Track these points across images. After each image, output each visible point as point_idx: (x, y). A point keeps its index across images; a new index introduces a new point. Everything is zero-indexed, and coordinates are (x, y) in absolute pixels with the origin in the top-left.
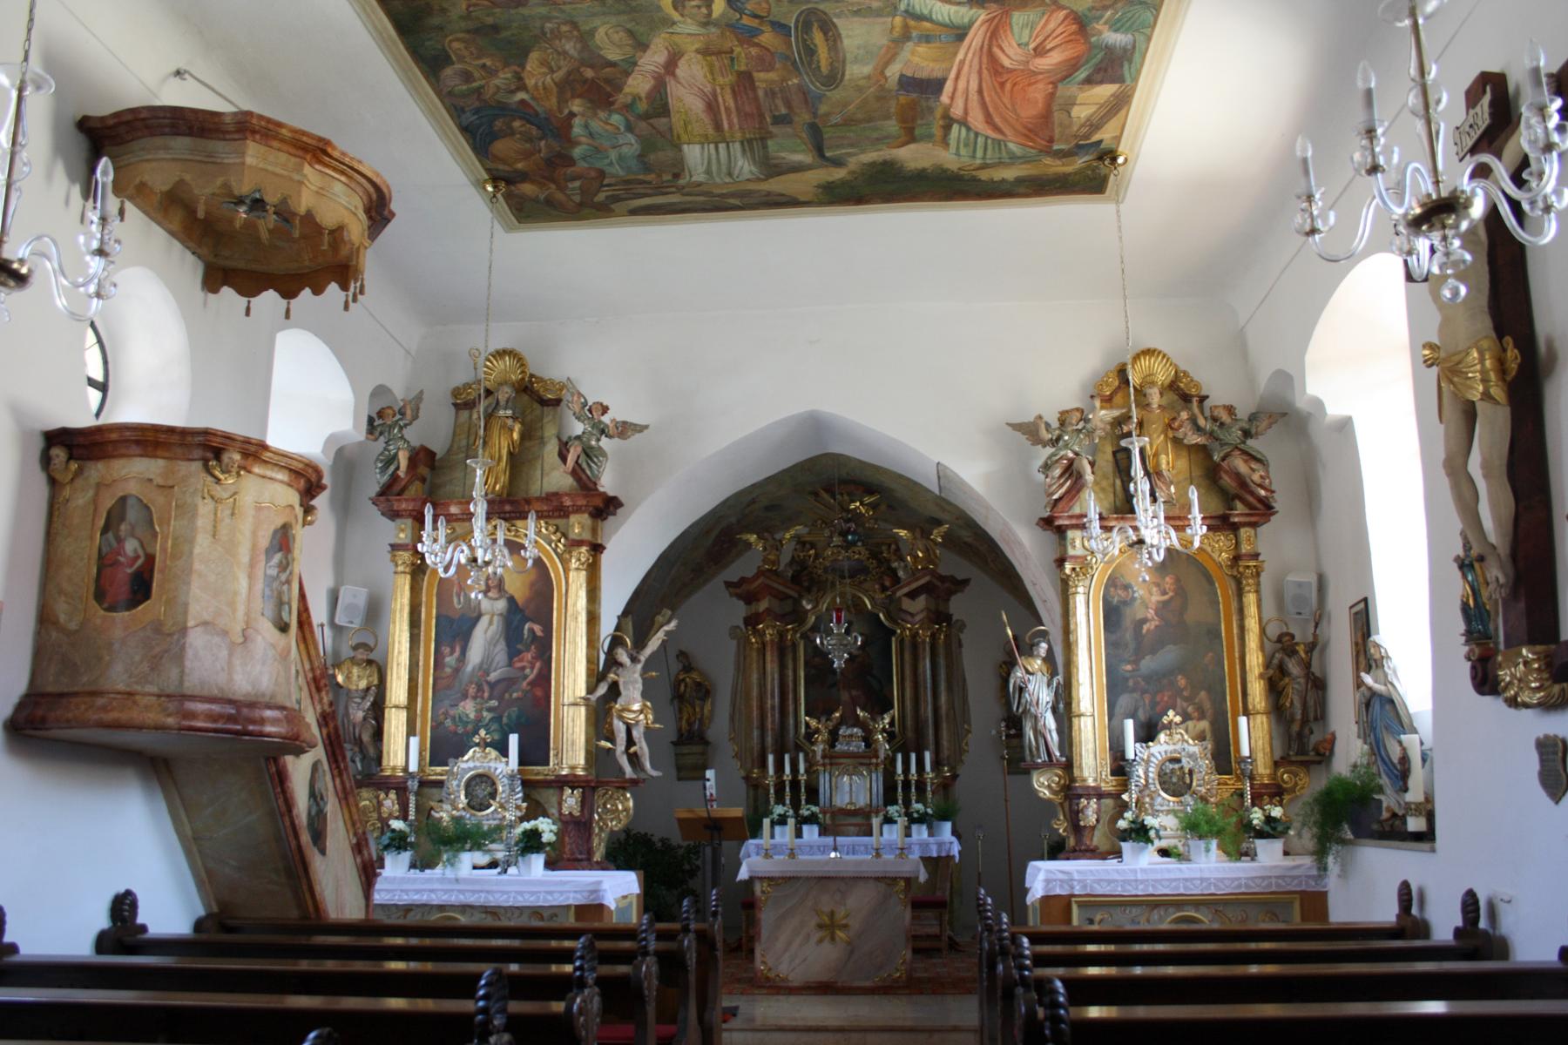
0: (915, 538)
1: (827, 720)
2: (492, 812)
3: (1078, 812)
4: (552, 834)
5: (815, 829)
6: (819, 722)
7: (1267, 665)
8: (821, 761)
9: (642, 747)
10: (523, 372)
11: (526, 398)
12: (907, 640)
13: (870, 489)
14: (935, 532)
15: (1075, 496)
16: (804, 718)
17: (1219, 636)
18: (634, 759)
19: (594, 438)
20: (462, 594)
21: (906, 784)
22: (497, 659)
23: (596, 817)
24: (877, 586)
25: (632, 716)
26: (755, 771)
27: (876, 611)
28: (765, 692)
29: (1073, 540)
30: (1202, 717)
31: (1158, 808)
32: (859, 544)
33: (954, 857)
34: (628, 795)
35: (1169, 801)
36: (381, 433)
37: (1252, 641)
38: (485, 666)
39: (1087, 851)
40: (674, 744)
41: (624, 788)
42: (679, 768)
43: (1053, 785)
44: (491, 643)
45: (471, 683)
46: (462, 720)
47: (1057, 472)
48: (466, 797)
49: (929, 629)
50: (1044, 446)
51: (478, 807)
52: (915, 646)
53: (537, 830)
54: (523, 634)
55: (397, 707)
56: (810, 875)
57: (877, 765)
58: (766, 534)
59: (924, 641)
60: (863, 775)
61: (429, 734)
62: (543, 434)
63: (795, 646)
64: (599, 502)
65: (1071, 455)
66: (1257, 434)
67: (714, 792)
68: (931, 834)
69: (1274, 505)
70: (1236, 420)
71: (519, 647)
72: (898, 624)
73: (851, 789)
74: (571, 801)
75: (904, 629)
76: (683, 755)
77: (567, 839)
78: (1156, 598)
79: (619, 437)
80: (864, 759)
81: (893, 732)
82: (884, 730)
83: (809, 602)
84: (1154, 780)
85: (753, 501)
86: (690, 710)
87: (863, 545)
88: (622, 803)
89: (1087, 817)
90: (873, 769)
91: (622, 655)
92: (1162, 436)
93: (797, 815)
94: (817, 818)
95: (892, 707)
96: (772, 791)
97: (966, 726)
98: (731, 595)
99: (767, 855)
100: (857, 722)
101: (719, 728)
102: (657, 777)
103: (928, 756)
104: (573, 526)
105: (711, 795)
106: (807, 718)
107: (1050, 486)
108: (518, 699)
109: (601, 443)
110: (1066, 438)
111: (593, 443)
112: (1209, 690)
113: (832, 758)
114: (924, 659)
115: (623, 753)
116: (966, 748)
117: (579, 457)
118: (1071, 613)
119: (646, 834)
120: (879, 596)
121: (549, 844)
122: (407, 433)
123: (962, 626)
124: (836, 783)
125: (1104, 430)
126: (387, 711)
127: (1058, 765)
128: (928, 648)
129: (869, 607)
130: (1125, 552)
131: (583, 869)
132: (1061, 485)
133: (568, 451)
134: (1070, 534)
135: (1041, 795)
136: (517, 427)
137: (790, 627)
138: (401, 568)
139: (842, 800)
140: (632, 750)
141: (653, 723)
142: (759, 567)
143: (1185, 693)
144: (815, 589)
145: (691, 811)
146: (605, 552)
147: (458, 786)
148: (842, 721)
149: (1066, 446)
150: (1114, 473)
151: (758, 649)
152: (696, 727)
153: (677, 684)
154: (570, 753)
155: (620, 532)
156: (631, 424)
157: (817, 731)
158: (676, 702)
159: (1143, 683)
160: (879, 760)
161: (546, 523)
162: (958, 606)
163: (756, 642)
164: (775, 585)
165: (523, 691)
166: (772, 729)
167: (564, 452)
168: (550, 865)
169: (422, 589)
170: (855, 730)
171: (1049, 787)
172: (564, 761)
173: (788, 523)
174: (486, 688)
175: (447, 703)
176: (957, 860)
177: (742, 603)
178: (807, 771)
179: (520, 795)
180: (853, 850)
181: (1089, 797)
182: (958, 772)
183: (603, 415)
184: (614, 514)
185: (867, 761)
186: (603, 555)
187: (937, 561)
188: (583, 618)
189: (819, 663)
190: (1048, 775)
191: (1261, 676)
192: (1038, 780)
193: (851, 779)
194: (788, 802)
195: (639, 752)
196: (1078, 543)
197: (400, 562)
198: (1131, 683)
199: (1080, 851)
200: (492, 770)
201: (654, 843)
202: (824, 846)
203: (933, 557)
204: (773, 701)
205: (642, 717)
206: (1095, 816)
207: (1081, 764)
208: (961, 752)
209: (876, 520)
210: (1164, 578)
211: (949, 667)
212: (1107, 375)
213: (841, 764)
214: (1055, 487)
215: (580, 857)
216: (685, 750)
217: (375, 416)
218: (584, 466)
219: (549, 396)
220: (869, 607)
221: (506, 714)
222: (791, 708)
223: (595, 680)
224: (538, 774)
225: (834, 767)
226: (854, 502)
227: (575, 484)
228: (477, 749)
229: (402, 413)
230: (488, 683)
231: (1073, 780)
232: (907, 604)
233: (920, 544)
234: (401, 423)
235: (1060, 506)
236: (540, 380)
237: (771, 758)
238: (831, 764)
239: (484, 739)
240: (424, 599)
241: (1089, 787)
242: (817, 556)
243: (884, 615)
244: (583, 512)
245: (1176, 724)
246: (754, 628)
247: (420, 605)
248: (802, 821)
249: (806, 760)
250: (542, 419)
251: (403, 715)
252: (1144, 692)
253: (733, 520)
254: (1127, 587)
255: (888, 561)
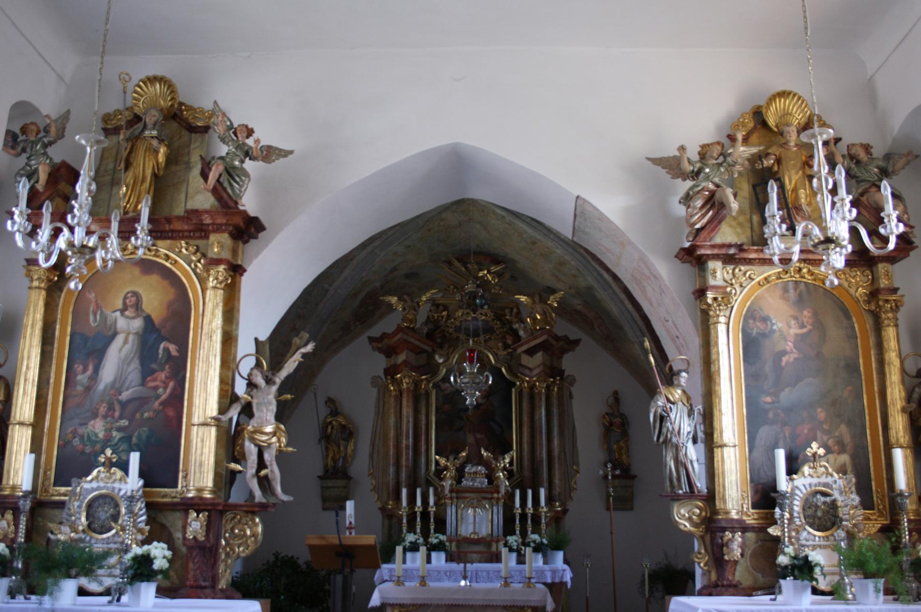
0: (534, 302)
1: (455, 459)
2: (113, 536)
3: (722, 546)
4: (165, 561)
5: (443, 555)
6: (448, 460)
7: (909, 399)
8: (449, 495)
9: (274, 471)
10: (173, 99)
11: (175, 125)
12: (526, 391)
13: (496, 259)
14: (552, 298)
15: (716, 227)
16: (434, 457)
17: (858, 370)
18: (265, 483)
19: (238, 158)
20: (99, 312)
21: (523, 516)
22: (130, 378)
23: (223, 542)
24: (500, 344)
25: (264, 438)
26: (391, 502)
27: (498, 365)
28: (401, 434)
29: (715, 272)
30: (842, 450)
31: (804, 542)
32: (486, 307)
33: (566, 583)
34: (257, 520)
35: (815, 536)
36: (24, 150)
37: (894, 377)
38: (117, 385)
39: (729, 586)
40: (320, 477)
41: (253, 513)
42: (324, 499)
43: (694, 517)
44: (124, 363)
45: (102, 401)
46: (90, 439)
47: (699, 203)
48: (87, 519)
49: (545, 381)
50: (684, 180)
51: (99, 529)
52: (532, 397)
53: (149, 555)
54: (157, 354)
55: (21, 424)
56: (440, 603)
57: (498, 499)
58: (405, 296)
59: (540, 392)
60: (485, 507)
61: (55, 453)
62: (189, 159)
63: (428, 394)
64: (238, 221)
65: (711, 186)
66: (894, 172)
67: (353, 520)
68: (545, 563)
69: (914, 240)
70: (873, 159)
71: (154, 366)
72: (517, 377)
73: (475, 520)
74: (196, 525)
75: (523, 381)
76: (328, 488)
77: (191, 565)
78: (794, 331)
79: (263, 161)
80: (487, 494)
81: (512, 470)
82: (505, 468)
83: (440, 357)
84: (798, 513)
85: (395, 269)
86: (336, 449)
87: (489, 308)
88: (251, 528)
89: (733, 550)
90: (495, 503)
91: (256, 376)
92: (801, 172)
93: (426, 543)
94: (444, 545)
95: (511, 449)
96: (405, 521)
97: (575, 467)
98: (374, 349)
99: (399, 582)
100: (481, 461)
101: (360, 466)
102: (287, 502)
103: (542, 492)
104: (213, 244)
105: (350, 523)
106: (437, 457)
107: (692, 216)
108: (149, 418)
109: (245, 166)
110: (707, 170)
111: (237, 163)
112: (849, 423)
113: (459, 493)
114: (540, 407)
115: (253, 476)
116: (575, 486)
117: (220, 175)
118: (712, 343)
119: (292, 557)
120: (502, 353)
121: (161, 571)
122: (50, 151)
123: (573, 381)
124: (462, 515)
125: (743, 165)
126: (10, 427)
127: (701, 497)
128: (543, 399)
129: (493, 361)
130: (764, 285)
131: (206, 597)
132: (704, 216)
133: (210, 169)
134: (712, 265)
135: (682, 527)
136: (163, 150)
137: (424, 377)
138: (36, 284)
139: (466, 530)
140: (263, 473)
141: (286, 446)
142: (398, 325)
143: (825, 427)
144: (446, 346)
145: (323, 538)
146: (245, 274)
147: (79, 507)
148: (468, 460)
149: (707, 178)
150: (751, 208)
151: (396, 396)
152: (340, 464)
153: (326, 425)
154: (198, 475)
155: (261, 256)
156: (277, 149)
157: (446, 468)
158: (323, 442)
159: (783, 415)
160: (500, 495)
161: (187, 243)
162: (568, 363)
163: (395, 390)
164: (412, 340)
165: (155, 411)
166: (406, 466)
167: (207, 170)
168: (162, 592)
169: (57, 306)
170: (479, 468)
171: (690, 519)
172: (191, 484)
173: (425, 288)
174: (117, 407)
175: (76, 421)
176: (569, 586)
177: (382, 357)
178: (436, 504)
179: (144, 518)
180: (476, 578)
181: (733, 531)
182: (567, 508)
183: (248, 137)
184: (256, 238)
185: (489, 496)
186: (243, 278)
187: (553, 323)
188: (218, 337)
189: (453, 398)
190: (689, 508)
191: (904, 410)
192: (679, 512)
193: (475, 511)
194: (418, 530)
195: (270, 476)
196: (719, 274)
197: (36, 277)
198: (771, 415)
199: (723, 586)
200: (116, 491)
201: (299, 566)
202: (450, 572)
203: (549, 319)
204: (407, 441)
205: (274, 439)
206: (740, 550)
207: (724, 496)
208: (571, 490)
209: (501, 287)
210: (801, 312)
211: (561, 414)
212: (742, 116)
213: (466, 498)
214: (697, 217)
215: (203, 584)
216: (330, 483)
217: (17, 131)
218: (226, 184)
219: (199, 124)
220: (493, 361)
221: (136, 434)
222: (423, 448)
223: (229, 400)
224: (165, 496)
225: (460, 501)
226: (481, 270)
227: (216, 203)
228: (102, 469)
229: (47, 130)
230: (120, 402)
231: (715, 512)
232: (526, 360)
233: (539, 307)
234: (46, 140)
235: (703, 235)
236: (190, 108)
237: (404, 492)
238: (457, 498)
239: (109, 459)
240: (59, 316)
241: (733, 520)
242: (449, 317)
243: (506, 369)
244: (223, 231)
245: (820, 456)
246: (393, 377)
247: (55, 322)
248: (432, 548)
249: (435, 495)
250: (189, 146)
251: (29, 432)
252: (785, 424)
253: (378, 285)
254: (765, 319)
255: (510, 322)
